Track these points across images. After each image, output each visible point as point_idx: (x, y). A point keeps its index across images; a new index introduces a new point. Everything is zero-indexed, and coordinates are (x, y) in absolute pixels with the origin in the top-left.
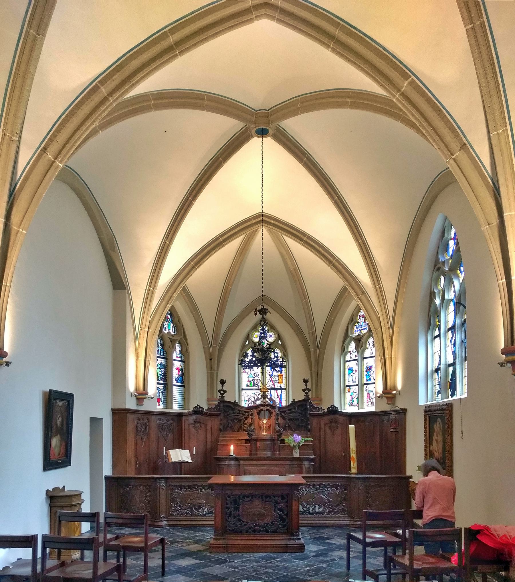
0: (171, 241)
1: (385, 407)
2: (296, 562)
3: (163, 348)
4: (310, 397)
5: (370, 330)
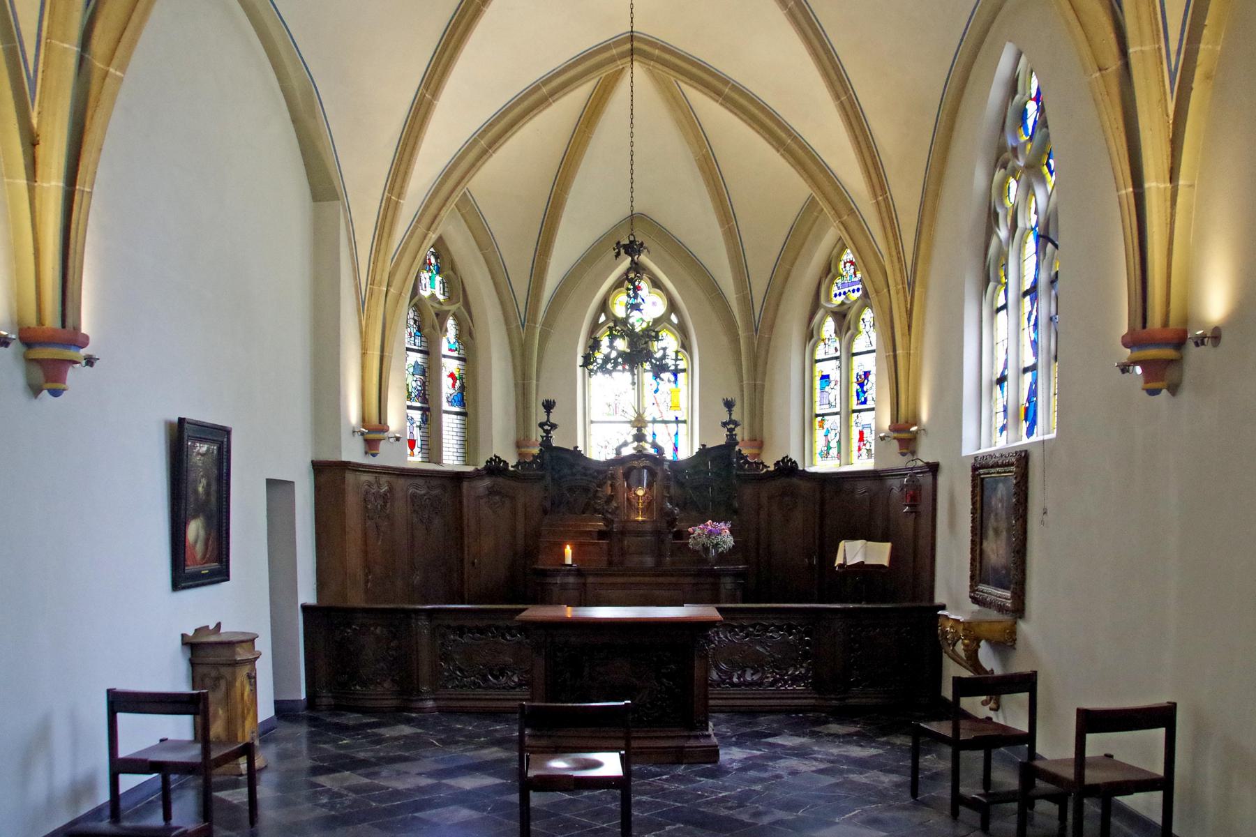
0: (435, 94)
1: (895, 460)
2: (701, 781)
3: (419, 330)
4: (739, 438)
5: (866, 295)
